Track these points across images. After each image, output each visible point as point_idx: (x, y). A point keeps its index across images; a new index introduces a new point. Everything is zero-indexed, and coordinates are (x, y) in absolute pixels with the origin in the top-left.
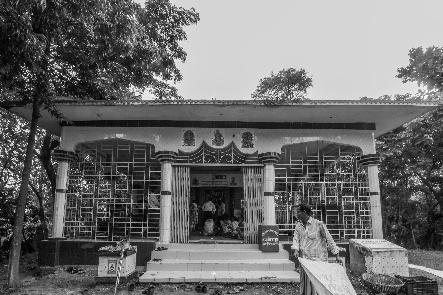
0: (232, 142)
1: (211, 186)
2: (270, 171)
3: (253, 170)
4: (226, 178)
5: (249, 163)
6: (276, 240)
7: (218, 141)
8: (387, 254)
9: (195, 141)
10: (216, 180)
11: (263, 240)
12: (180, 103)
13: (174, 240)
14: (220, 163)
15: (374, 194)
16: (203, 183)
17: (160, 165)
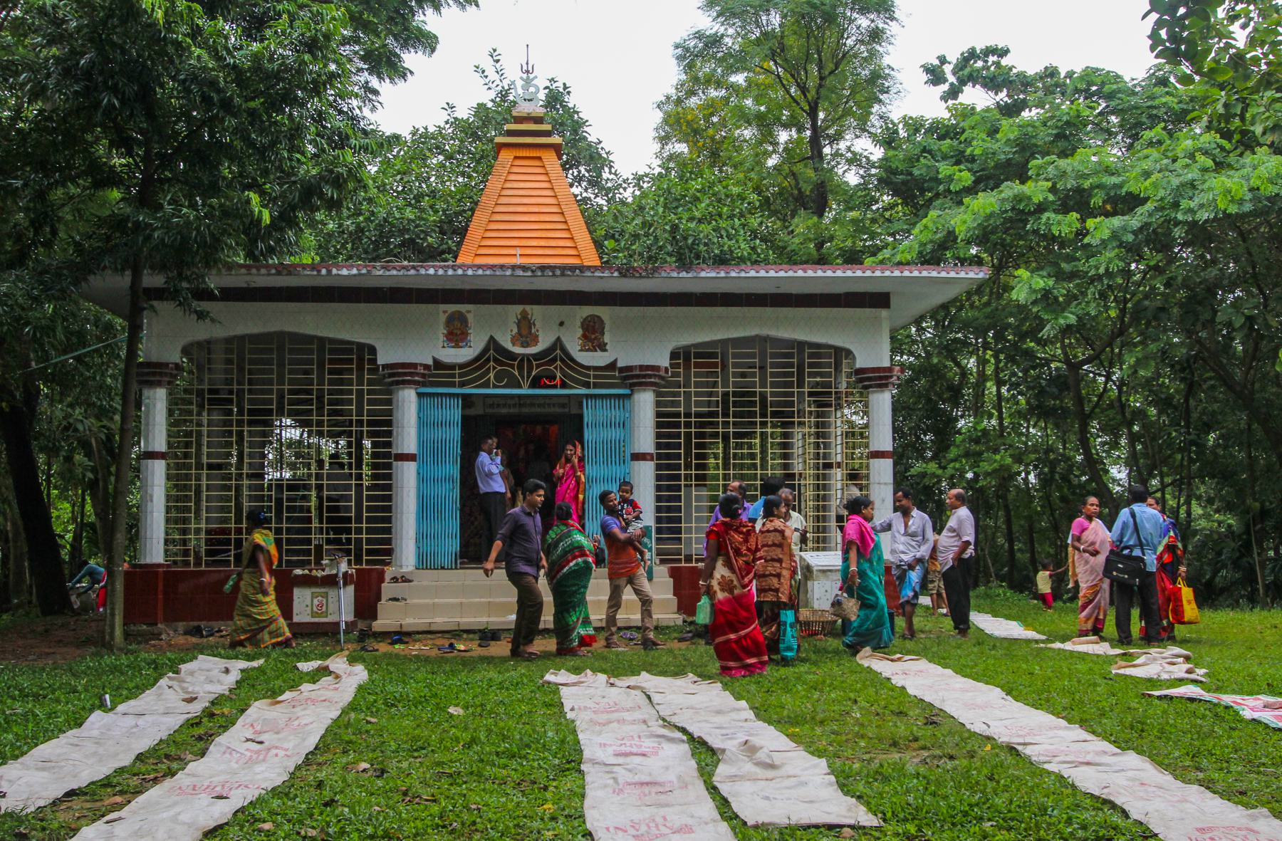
0: (559, 339)
2: (645, 403)
3: (607, 402)
5: (596, 386)
7: (526, 333)
9: (471, 337)
13: (424, 563)
17: (390, 393)
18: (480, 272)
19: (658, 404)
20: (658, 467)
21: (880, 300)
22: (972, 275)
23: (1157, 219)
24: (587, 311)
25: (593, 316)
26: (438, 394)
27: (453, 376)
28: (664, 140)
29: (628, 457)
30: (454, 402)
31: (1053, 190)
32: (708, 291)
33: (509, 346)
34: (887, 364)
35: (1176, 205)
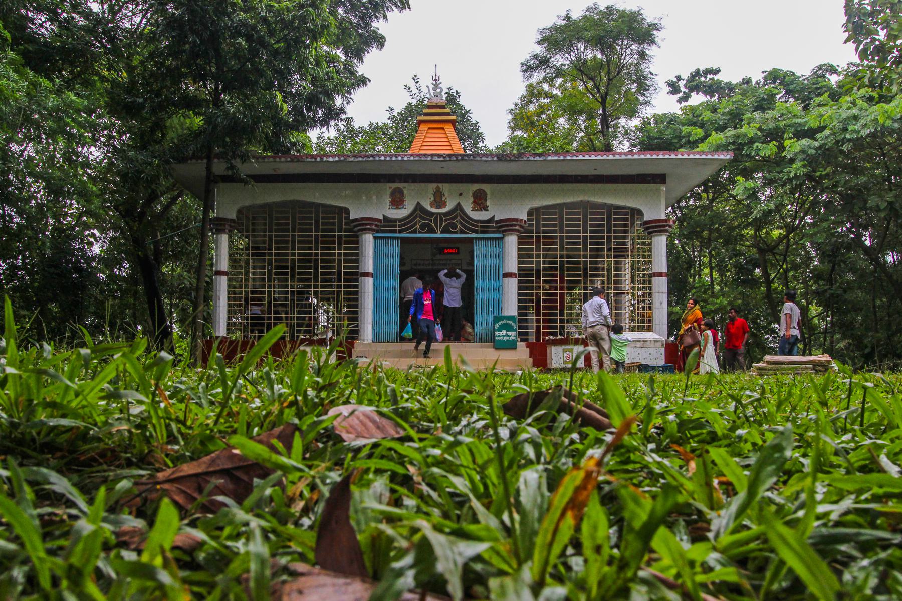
0: (459, 204)
1: (430, 267)
2: (512, 242)
4: (458, 253)
5: (482, 232)
6: (513, 333)
7: (439, 201)
8: (639, 344)
9: (406, 203)
10: (439, 257)
11: (496, 333)
12: (388, 159)
13: (377, 338)
14: (442, 233)
15: (660, 275)
16: (415, 262)
17: (357, 237)
18: (412, 158)
19: (520, 243)
20: (520, 282)
21: (661, 179)
22: (722, 157)
23: (830, 142)
24: (476, 187)
25: (479, 190)
26: (385, 238)
27: (395, 226)
28: (513, 129)
29: (501, 276)
30: (396, 242)
31: (760, 129)
32: (551, 173)
33: (429, 208)
34: (663, 217)
35: (845, 130)
